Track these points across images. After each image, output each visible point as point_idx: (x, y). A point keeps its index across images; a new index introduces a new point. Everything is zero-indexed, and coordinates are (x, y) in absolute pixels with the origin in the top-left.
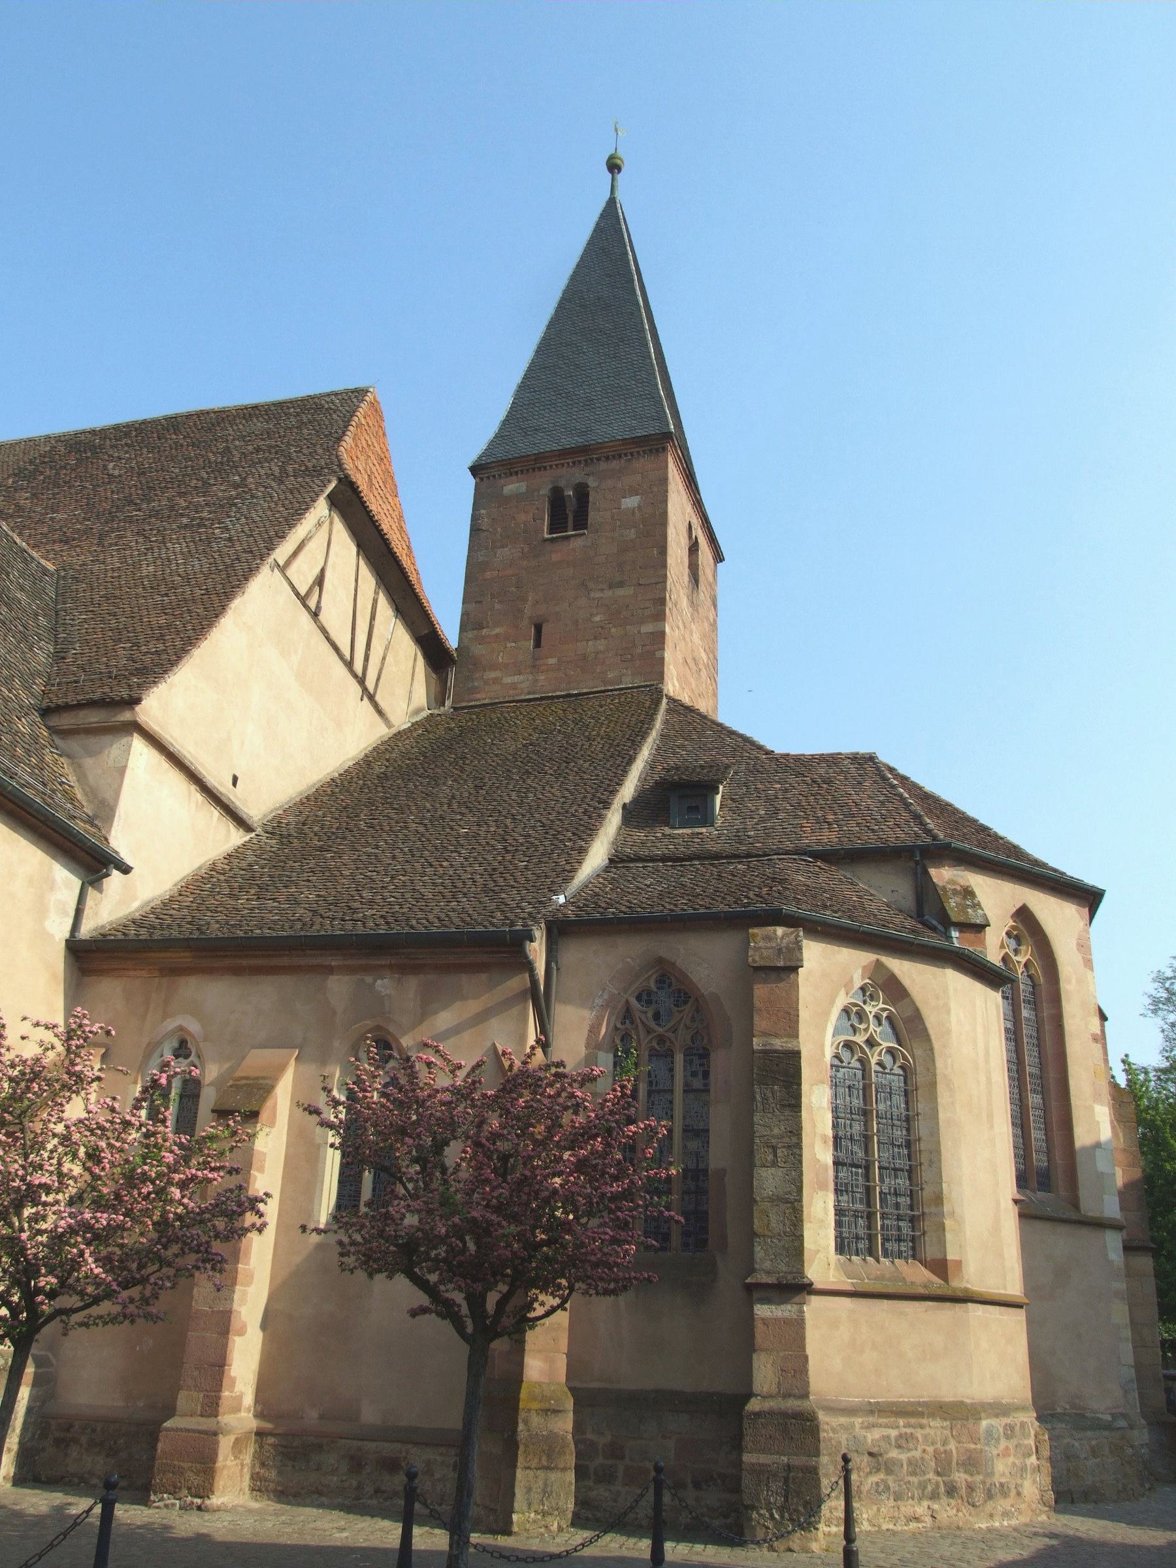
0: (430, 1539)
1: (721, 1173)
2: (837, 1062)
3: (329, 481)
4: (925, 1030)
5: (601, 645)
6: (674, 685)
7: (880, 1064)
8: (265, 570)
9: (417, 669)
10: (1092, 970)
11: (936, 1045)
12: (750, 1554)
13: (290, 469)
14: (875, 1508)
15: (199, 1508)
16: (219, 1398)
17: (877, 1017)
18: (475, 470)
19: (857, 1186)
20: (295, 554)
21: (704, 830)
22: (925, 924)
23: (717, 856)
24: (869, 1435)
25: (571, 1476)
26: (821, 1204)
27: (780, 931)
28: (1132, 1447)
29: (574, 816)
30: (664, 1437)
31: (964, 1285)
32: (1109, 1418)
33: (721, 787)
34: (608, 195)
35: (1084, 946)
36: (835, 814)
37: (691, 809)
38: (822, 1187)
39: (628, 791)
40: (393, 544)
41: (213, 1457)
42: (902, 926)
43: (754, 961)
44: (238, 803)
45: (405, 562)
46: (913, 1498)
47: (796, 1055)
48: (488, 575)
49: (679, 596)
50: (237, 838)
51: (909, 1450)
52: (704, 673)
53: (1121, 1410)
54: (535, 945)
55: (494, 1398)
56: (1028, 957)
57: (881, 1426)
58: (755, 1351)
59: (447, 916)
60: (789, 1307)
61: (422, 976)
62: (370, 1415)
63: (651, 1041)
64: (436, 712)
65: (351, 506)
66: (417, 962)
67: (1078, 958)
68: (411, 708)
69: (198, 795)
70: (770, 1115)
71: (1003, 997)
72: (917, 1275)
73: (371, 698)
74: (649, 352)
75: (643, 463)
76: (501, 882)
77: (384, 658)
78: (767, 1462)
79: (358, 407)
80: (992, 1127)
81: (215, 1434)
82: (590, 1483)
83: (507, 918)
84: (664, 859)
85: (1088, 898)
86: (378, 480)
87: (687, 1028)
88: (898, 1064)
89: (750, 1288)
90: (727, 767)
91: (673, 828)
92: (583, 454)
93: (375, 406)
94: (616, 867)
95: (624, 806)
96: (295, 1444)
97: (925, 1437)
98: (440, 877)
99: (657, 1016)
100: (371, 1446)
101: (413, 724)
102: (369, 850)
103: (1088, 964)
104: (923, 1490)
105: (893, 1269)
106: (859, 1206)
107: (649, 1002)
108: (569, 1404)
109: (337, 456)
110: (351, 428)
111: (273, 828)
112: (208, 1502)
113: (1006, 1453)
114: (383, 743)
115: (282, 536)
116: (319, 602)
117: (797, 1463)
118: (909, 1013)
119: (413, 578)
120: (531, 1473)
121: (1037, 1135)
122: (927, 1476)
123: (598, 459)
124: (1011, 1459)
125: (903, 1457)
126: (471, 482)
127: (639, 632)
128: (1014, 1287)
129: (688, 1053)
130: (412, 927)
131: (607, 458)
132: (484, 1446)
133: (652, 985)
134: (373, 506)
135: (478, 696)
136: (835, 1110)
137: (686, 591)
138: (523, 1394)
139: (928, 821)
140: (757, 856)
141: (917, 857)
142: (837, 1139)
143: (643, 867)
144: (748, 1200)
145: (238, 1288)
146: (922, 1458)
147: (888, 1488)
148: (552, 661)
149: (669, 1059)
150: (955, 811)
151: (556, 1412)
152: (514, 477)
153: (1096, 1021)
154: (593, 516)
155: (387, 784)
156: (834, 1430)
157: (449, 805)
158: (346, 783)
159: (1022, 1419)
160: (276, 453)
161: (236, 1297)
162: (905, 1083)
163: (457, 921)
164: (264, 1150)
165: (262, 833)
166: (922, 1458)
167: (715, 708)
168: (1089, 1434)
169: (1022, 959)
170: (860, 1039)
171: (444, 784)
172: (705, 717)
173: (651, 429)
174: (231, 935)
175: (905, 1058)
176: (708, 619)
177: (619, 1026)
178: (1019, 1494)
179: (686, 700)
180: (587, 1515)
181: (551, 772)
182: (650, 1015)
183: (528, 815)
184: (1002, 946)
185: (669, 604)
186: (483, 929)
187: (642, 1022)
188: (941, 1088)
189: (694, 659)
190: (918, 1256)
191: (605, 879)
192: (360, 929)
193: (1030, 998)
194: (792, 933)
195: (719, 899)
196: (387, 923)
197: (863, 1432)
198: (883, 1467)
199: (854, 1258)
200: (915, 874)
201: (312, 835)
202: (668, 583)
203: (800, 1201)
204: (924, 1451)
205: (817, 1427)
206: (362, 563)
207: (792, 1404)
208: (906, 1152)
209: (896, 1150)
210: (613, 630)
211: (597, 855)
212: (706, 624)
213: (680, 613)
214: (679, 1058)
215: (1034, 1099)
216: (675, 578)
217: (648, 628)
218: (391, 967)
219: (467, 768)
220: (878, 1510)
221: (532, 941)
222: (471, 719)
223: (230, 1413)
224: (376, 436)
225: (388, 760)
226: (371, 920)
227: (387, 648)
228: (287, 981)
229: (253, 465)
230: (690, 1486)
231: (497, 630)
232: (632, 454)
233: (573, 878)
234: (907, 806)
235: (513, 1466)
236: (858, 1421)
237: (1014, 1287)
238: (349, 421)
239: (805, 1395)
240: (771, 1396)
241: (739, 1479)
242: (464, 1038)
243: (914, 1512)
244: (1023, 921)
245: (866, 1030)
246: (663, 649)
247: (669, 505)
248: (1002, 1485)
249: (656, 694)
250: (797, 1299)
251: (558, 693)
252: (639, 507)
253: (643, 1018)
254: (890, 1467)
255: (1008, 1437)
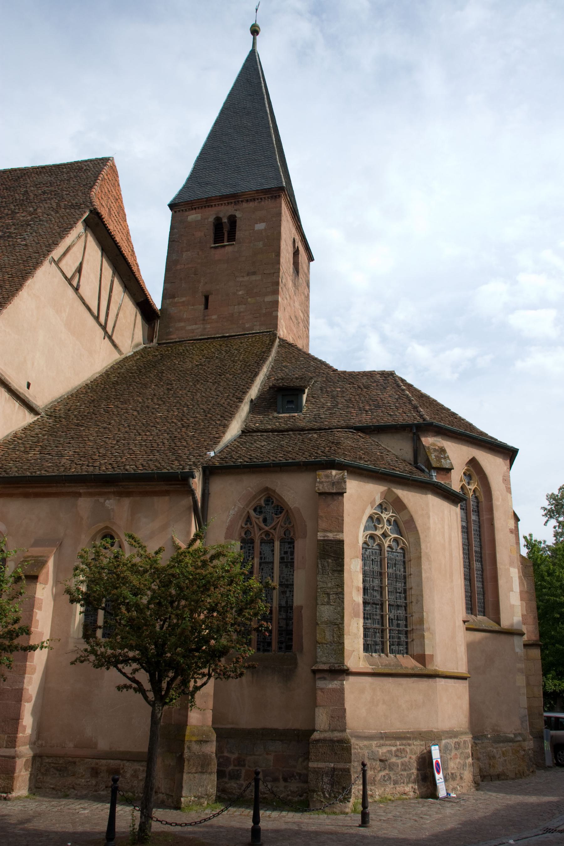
0: (127, 816)
1: (301, 608)
2: (365, 546)
3: (85, 212)
4: (416, 527)
5: (242, 308)
6: (283, 331)
7: (389, 547)
8: (46, 263)
9: (137, 321)
10: (510, 493)
11: (422, 536)
12: (312, 816)
13: (62, 204)
14: (383, 789)
15: (5, 799)
16: (16, 737)
17: (389, 521)
18: (172, 206)
19: (376, 615)
20: (65, 254)
21: (296, 414)
22: (418, 468)
23: (303, 430)
24: (380, 750)
25: (214, 777)
26: (356, 625)
27: (334, 472)
28: (524, 750)
29: (222, 406)
30: (267, 754)
31: (435, 668)
32: (512, 736)
33: (306, 391)
34: (250, 48)
35: (506, 480)
36: (370, 405)
37: (290, 402)
38: (356, 615)
39: (254, 392)
40: (123, 249)
41: (13, 770)
42: (401, 469)
43: (319, 489)
44: (30, 398)
45: (130, 259)
46: (403, 783)
47: (341, 543)
48: (179, 267)
49: (287, 280)
50: (30, 418)
51: (402, 758)
52: (301, 325)
53: (520, 731)
54: (196, 480)
55: (169, 737)
56: (476, 486)
57: (387, 745)
58: (317, 706)
59: (147, 463)
60: (336, 682)
61: (131, 498)
62: (103, 745)
63: (261, 535)
64: (148, 346)
65: (98, 227)
66: (131, 490)
67: (503, 487)
68: (134, 343)
69: (6, 394)
70: (326, 576)
71: (461, 509)
72: (408, 663)
73: (110, 338)
74: (272, 140)
75: (268, 204)
76: (178, 444)
77: (117, 315)
78: (322, 766)
79: (103, 169)
80: (452, 581)
81: (14, 758)
82: (226, 780)
83: (181, 465)
84: (273, 431)
85: (509, 453)
86: (114, 211)
87: (282, 527)
88: (400, 547)
89: (314, 672)
90: (311, 378)
91: (279, 413)
92: (234, 198)
93: (113, 169)
94: (245, 436)
95: (252, 401)
96: (61, 762)
97: (411, 750)
98: (145, 441)
99: (265, 520)
100: (104, 762)
101: (135, 353)
102: (105, 425)
103: (509, 490)
104: (409, 778)
105: (395, 660)
106: (377, 626)
107: (261, 512)
108: (214, 737)
109: (90, 198)
110: (98, 181)
111: (51, 412)
112: (10, 796)
113: (455, 757)
114: (117, 364)
115: (56, 244)
116: (79, 282)
117: (338, 767)
118: (406, 518)
119: (134, 269)
120: (191, 776)
121: (477, 584)
122: (412, 771)
123: (242, 201)
124: (458, 760)
125: (399, 761)
126: (169, 213)
127: (264, 301)
128: (462, 668)
129: (282, 541)
130: (127, 470)
131: (247, 201)
132: (160, 765)
133: (262, 503)
134: (111, 227)
135: (172, 337)
136: (365, 574)
137: (291, 277)
138: (188, 732)
139: (422, 410)
140: (325, 429)
141: (415, 430)
142: (365, 590)
143: (261, 435)
144: (315, 624)
145: (26, 675)
146: (409, 762)
147: (390, 778)
148: (214, 317)
149: (272, 544)
150: (438, 404)
151: (206, 742)
152: (194, 211)
153: (512, 522)
154: (239, 234)
155: (118, 387)
156: (360, 748)
157: (152, 399)
158: (94, 387)
159: (464, 739)
160: (55, 195)
161: (26, 681)
162: (404, 557)
163: (153, 467)
164: (42, 598)
165: (45, 416)
166: (409, 762)
167: (308, 345)
168: (501, 745)
169: (472, 487)
170: (379, 533)
171: (150, 387)
172: (300, 350)
173: (273, 184)
174: (23, 475)
175: (404, 543)
176: (304, 293)
177: (244, 525)
178: (461, 778)
179: (290, 340)
180: (226, 798)
181: (211, 381)
182: (261, 520)
183: (196, 406)
184: (461, 481)
185: (281, 285)
186: (167, 471)
187: (256, 523)
188: (424, 559)
189: (296, 317)
190: (409, 653)
191: (238, 442)
192: (97, 472)
193: (476, 509)
194: (341, 474)
195: (300, 454)
196: (113, 468)
197: (377, 749)
198: (388, 767)
199: (374, 654)
200: (413, 440)
201: (73, 416)
202: (281, 273)
203: (343, 623)
204: (410, 758)
205: (350, 747)
206: (104, 260)
207: (337, 735)
208: (403, 595)
209: (398, 594)
210: (249, 299)
211: (234, 429)
212: (303, 297)
213: (288, 290)
214: (277, 544)
215: (476, 565)
216: (285, 270)
217: (268, 299)
218: (114, 493)
219: (164, 378)
220: (385, 790)
221: (193, 478)
222: (168, 350)
223: (23, 746)
224: (114, 185)
225: (119, 373)
226: (103, 467)
227: (119, 309)
228: (55, 501)
229: (41, 201)
230: (281, 780)
231: (184, 299)
232: (261, 199)
233: (219, 442)
234: (410, 401)
235: (181, 772)
236: (374, 743)
237: (462, 668)
238: (97, 177)
239: (344, 730)
240: (325, 731)
241: (307, 776)
242: (160, 534)
243: (404, 790)
244: (473, 467)
245: (382, 528)
246: (277, 311)
247: (282, 229)
248: (452, 774)
249: (273, 336)
250: (340, 678)
251: (218, 336)
252: (265, 229)
253: (257, 521)
254: (391, 767)
255: (456, 749)
